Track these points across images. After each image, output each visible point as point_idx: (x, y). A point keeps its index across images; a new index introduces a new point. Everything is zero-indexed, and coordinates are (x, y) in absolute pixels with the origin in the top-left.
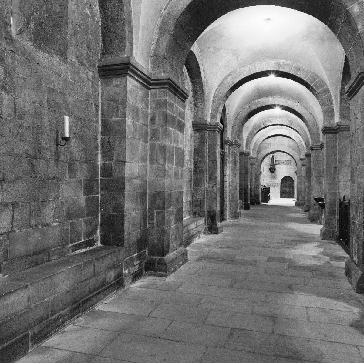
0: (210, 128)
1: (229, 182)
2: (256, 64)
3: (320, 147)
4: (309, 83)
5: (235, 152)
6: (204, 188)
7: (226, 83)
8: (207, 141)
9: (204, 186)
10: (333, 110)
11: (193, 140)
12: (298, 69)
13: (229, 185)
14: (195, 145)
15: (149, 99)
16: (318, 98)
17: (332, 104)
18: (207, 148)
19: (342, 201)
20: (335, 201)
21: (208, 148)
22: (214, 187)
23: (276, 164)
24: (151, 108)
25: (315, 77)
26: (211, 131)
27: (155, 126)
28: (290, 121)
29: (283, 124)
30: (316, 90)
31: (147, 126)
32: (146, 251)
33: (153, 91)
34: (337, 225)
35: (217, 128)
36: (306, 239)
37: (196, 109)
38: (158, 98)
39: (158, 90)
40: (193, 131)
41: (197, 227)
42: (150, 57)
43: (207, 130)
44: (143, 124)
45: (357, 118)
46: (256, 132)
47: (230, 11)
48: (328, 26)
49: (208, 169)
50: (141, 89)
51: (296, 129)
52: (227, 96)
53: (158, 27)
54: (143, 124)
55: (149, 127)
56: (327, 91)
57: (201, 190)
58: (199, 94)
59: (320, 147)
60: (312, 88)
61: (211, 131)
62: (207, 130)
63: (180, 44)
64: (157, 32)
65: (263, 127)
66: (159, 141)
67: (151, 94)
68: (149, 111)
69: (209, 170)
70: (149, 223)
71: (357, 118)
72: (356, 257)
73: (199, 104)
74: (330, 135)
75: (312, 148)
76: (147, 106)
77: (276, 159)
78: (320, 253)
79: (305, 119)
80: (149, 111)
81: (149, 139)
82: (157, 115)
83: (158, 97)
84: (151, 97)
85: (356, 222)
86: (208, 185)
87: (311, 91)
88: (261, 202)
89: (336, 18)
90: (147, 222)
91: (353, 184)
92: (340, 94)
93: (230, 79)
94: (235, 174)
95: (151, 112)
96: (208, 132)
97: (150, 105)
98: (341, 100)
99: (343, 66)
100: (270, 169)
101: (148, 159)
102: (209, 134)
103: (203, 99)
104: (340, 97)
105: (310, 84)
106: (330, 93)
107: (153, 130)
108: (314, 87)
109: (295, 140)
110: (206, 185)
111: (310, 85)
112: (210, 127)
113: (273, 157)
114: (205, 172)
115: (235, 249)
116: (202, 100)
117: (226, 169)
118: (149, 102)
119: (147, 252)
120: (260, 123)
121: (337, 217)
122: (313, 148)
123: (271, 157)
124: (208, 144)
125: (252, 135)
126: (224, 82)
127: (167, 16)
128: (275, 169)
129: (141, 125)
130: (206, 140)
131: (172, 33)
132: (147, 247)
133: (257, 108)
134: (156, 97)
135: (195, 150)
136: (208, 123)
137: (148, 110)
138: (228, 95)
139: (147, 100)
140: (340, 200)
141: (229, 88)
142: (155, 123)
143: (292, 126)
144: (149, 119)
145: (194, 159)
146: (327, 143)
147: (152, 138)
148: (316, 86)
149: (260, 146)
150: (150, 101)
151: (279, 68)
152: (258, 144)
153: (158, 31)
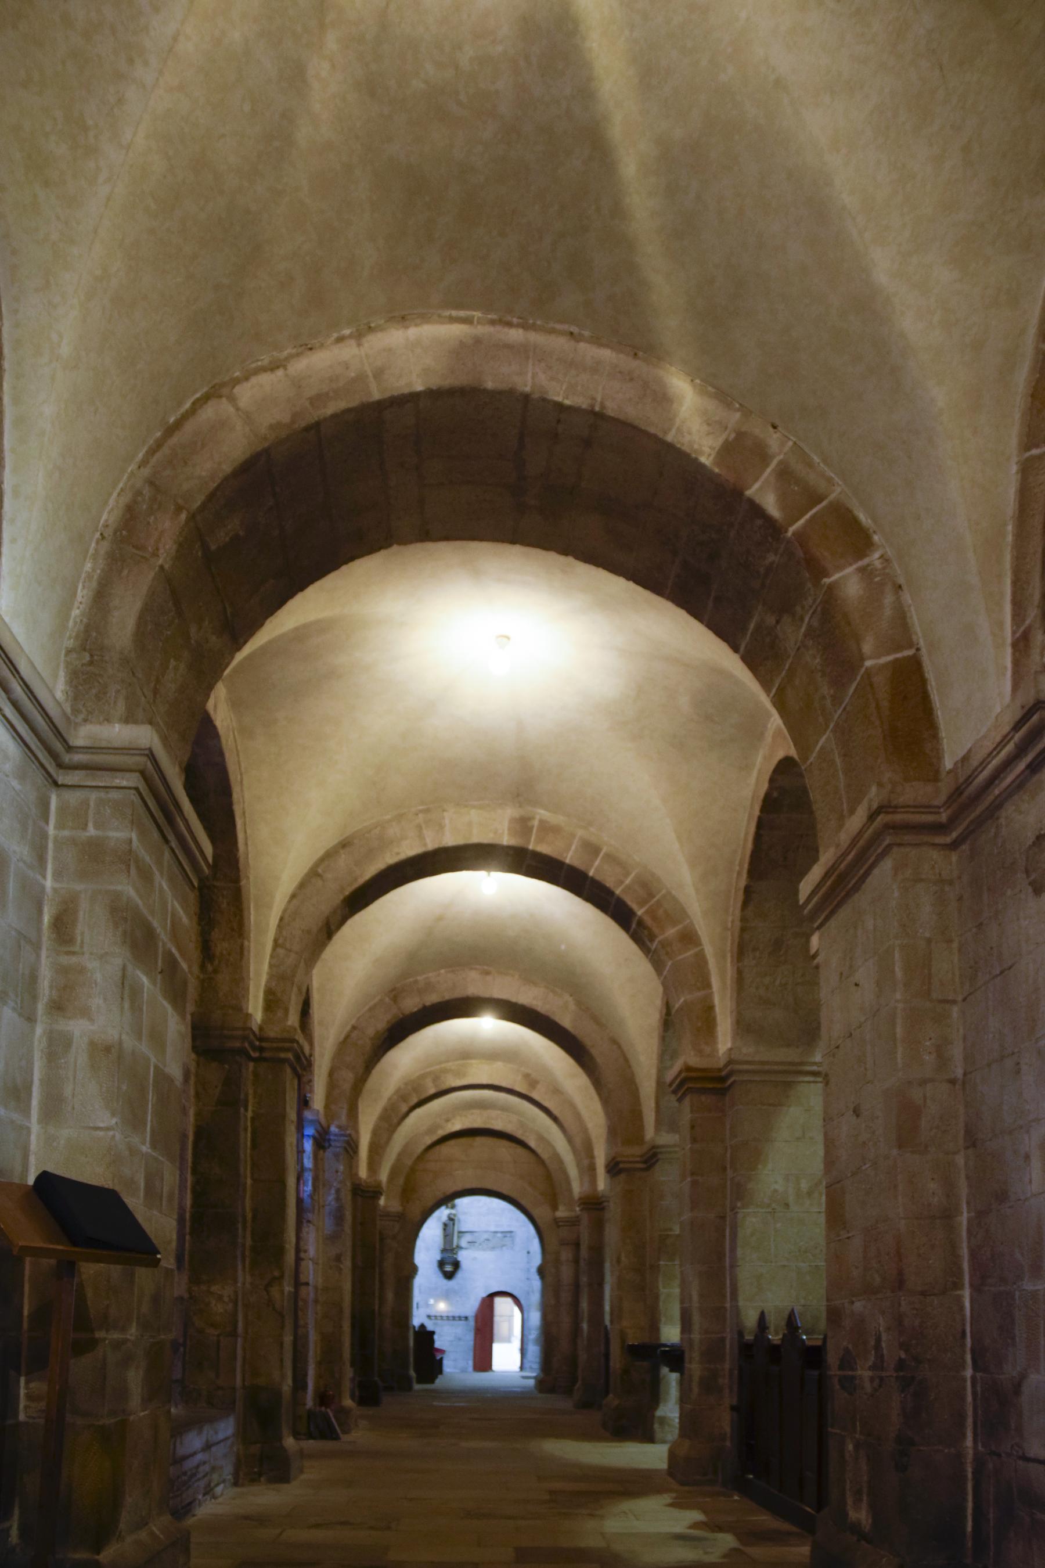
0: (261, 1049)
1: (316, 1288)
2: (445, 814)
3: (645, 1162)
4: (629, 903)
5: (337, 1172)
6: (236, 1292)
7: (329, 876)
8: (247, 1101)
9: (236, 1281)
10: (709, 1009)
11: (192, 1092)
12: (592, 849)
13: (316, 1301)
14: (198, 1114)
15: (51, 830)
16: (658, 965)
17: (708, 986)
18: (246, 1130)
19: (749, 1337)
20: (723, 1340)
21: (249, 1129)
22: (275, 1291)
23: (459, 1247)
24: (58, 875)
25: (647, 886)
26: (265, 1060)
27: (74, 953)
28: (527, 1076)
29: (504, 1084)
30: (656, 930)
31: (37, 947)
32: (11, 1527)
33: (73, 798)
34: (728, 1429)
35: (287, 1050)
36: (633, 1484)
37: (210, 968)
38: (92, 831)
39: (93, 796)
40: (193, 1056)
41: (208, 1447)
42: (63, 652)
43: (251, 1058)
44: (19, 933)
45: (856, 985)
46: (404, 1108)
47: (390, 545)
48: (744, 659)
49: (249, 1216)
50: (22, 777)
51: (546, 1104)
52: (329, 929)
53: (109, 533)
54: (19, 933)
55: (44, 953)
56: (689, 938)
57: (220, 1298)
58: (224, 906)
59: (645, 1162)
60: (640, 923)
61: (265, 1060)
62: (251, 1058)
63: (193, 630)
64: (102, 552)
65: (432, 1091)
66: (91, 1020)
67: (62, 810)
68: (49, 883)
69: (254, 1217)
70: (29, 1397)
71: (856, 985)
72: (864, 1505)
73: (221, 947)
74: (703, 1098)
75: (617, 1163)
76: (41, 859)
77: (463, 1230)
78: (695, 1525)
79: (592, 1058)
80: (49, 883)
81: (41, 1007)
82: (84, 905)
83: (91, 826)
84: (60, 826)
85: (859, 1372)
86: (249, 1279)
87: (636, 938)
88: (414, 1380)
89: (778, 622)
90: (22, 1392)
91: (839, 1236)
92: (735, 950)
93: (343, 860)
94: (338, 1258)
95: (55, 890)
96: (251, 1065)
97: (55, 858)
98: (740, 973)
99: (750, 845)
100: (441, 1264)
101: (35, 1102)
102: (256, 1075)
103: (239, 929)
104: (738, 961)
105: (634, 906)
106: (701, 945)
107: (63, 971)
108: (648, 921)
109: (539, 1151)
110: (240, 1279)
111: (631, 913)
112: (264, 1044)
113: (451, 1219)
114: (240, 1226)
115: (371, 1528)
116: (233, 930)
117: (308, 1233)
118: (51, 845)
119: (14, 1532)
120: (423, 1077)
121: (729, 1399)
122: (621, 1166)
123: (445, 1218)
124: (250, 1114)
125: (391, 1119)
126: (320, 871)
127: (147, 491)
128: (457, 1265)
129: (13, 933)
130: (247, 1095)
131: (166, 567)
132: (16, 1512)
133: (425, 1008)
134: (85, 827)
135: (200, 1132)
136: (255, 1028)
137: (44, 877)
138: (333, 927)
139: (44, 836)
140: (741, 1334)
141: (342, 897)
142: (71, 941)
143: (535, 1095)
144: (46, 919)
145: (194, 1171)
146: (693, 1127)
147: (57, 1007)
148: (654, 918)
149: (413, 1170)
150: (56, 840)
151: (529, 842)
152: (409, 1162)
153: (105, 546)
